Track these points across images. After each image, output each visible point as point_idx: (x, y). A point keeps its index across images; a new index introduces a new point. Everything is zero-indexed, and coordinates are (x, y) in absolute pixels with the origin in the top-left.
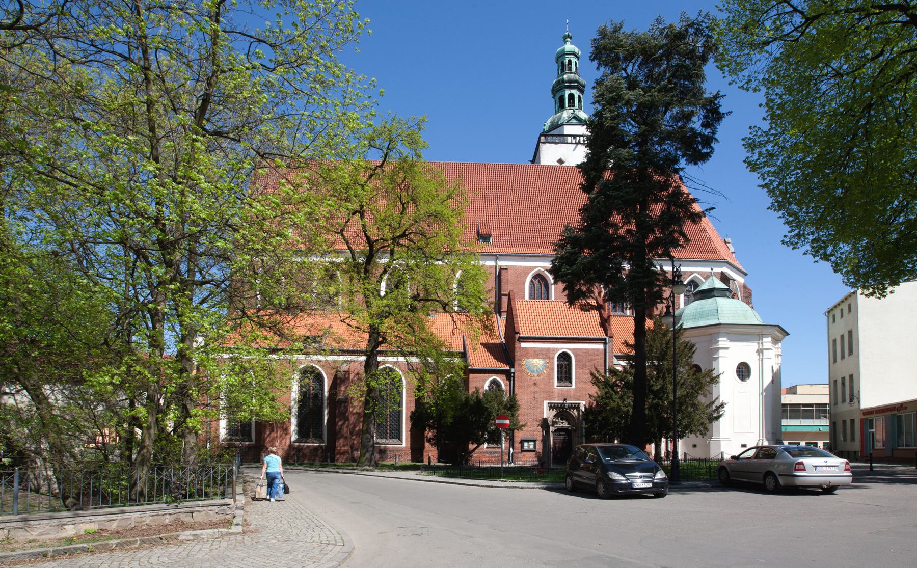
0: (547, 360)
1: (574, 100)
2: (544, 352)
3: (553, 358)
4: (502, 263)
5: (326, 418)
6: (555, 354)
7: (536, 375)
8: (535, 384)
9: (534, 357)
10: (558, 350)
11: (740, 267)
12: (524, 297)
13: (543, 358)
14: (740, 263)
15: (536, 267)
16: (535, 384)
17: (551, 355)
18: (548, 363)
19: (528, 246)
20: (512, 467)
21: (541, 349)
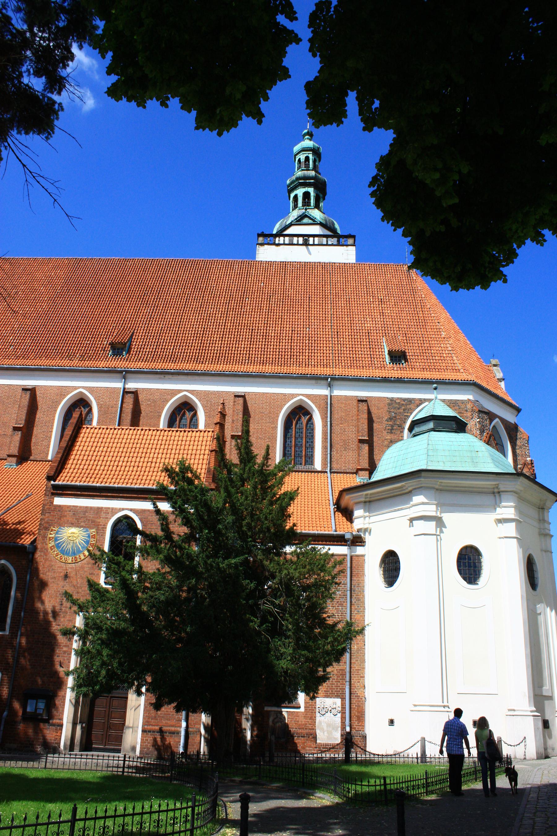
0: (93, 531)
1: (309, 198)
2: (91, 515)
3: (105, 528)
4: (132, 385)
5: (489, 780)
6: (108, 519)
7: (70, 560)
8: (66, 576)
9: (72, 525)
10: (114, 511)
11: (514, 403)
12: (310, 459)
13: (87, 527)
14: (514, 399)
15: (180, 391)
16: (66, 576)
17: (101, 521)
18: (93, 537)
19: (173, 358)
20: (137, 777)
21: (87, 509)
